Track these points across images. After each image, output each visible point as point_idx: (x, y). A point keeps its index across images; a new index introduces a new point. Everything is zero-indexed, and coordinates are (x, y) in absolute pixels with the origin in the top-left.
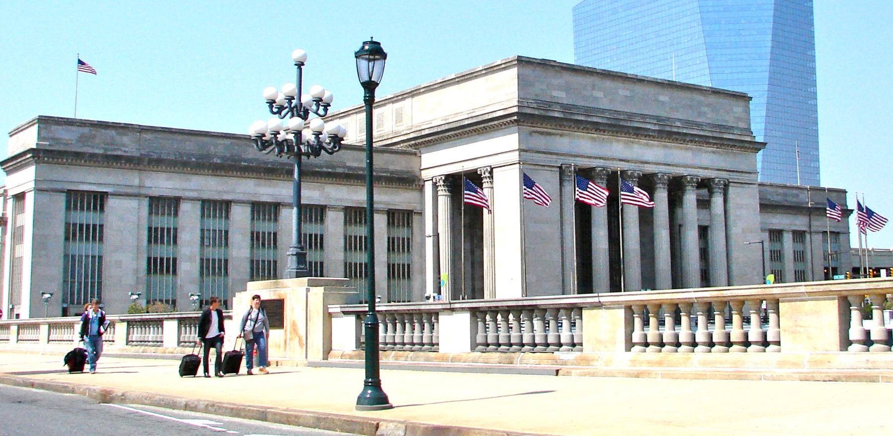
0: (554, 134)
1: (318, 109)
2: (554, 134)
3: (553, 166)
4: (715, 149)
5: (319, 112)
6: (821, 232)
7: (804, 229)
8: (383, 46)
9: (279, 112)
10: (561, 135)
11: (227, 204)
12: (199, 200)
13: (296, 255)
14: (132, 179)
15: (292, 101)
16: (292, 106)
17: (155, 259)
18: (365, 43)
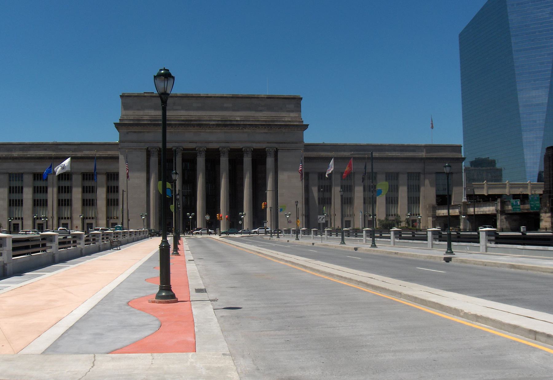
0: (144, 132)
2: (144, 132)
3: (142, 149)
4: (267, 131)
6: (435, 173)
7: (419, 171)
8: (171, 71)
10: (148, 132)
11: (398, 174)
12: (7, 174)
17: (87, 200)
18: (161, 70)
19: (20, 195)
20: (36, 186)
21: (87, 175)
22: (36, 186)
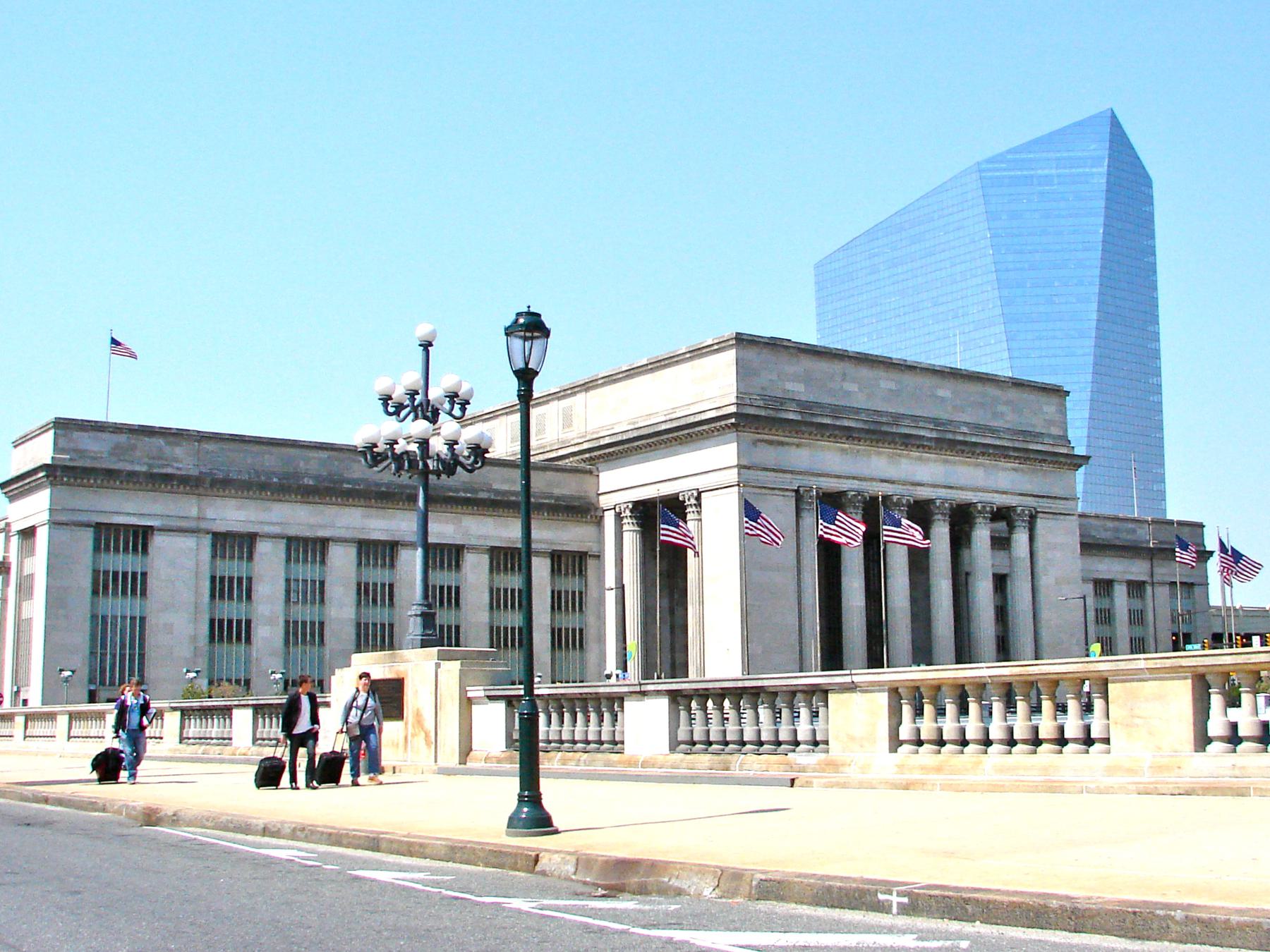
0: (787, 444)
1: (452, 409)
2: (787, 444)
3: (787, 490)
5: (453, 412)
9: (397, 413)
10: (798, 446)
11: (324, 543)
13: (420, 615)
14: (187, 507)
15: (416, 397)
16: (416, 403)
19: (110, 600)
20: (102, 569)
21: (559, 557)
22: (102, 569)
